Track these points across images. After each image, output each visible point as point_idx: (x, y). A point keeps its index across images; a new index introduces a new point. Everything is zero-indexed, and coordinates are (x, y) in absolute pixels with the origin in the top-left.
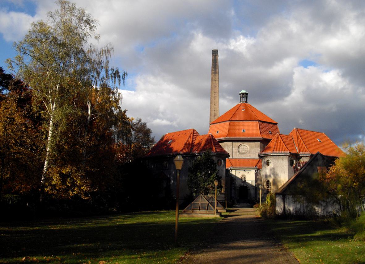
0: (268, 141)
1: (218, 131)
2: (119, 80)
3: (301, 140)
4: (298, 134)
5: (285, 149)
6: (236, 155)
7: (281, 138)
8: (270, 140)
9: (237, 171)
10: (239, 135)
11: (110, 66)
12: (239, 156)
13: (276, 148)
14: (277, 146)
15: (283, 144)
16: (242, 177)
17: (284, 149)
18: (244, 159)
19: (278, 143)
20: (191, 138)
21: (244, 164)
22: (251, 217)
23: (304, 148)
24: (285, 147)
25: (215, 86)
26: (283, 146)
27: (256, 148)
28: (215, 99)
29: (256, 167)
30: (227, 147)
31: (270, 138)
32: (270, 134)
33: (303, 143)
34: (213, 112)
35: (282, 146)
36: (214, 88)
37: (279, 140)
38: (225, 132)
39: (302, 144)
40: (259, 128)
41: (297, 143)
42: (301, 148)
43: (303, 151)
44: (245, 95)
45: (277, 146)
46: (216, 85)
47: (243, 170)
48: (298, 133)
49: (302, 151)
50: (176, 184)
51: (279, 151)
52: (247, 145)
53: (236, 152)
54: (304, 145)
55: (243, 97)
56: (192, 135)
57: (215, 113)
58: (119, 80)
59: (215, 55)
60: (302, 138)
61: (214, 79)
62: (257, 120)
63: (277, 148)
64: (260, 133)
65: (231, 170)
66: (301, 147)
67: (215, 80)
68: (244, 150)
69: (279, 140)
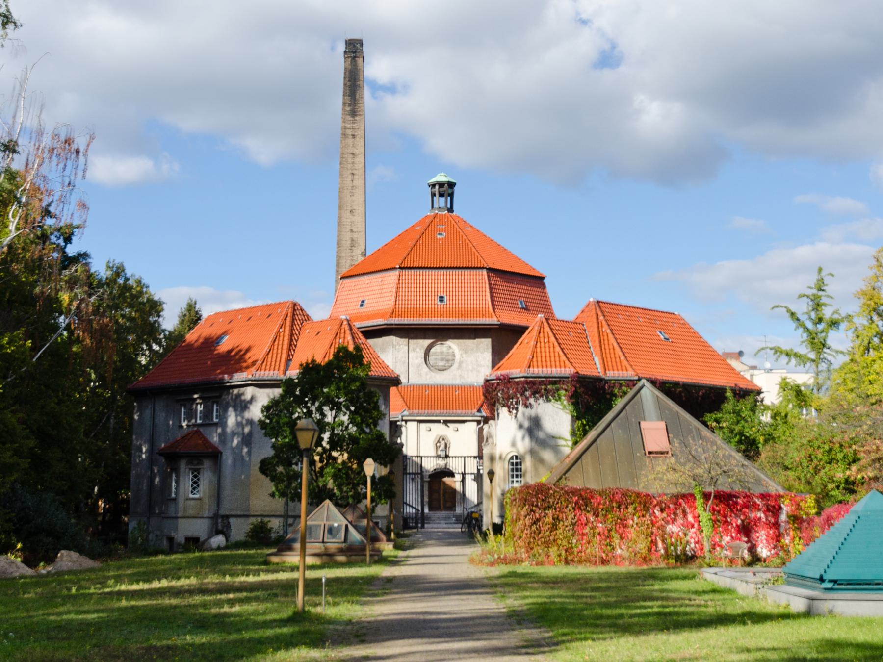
0: (518, 331)
1: (363, 301)
3: (611, 336)
4: (601, 318)
5: (562, 364)
7: (551, 329)
8: (527, 328)
9: (423, 425)
12: (428, 376)
13: (535, 359)
14: (539, 355)
15: (558, 349)
16: (438, 442)
17: (558, 364)
19: (543, 345)
20: (288, 328)
21: (441, 404)
23: (618, 360)
24: (563, 358)
25: (353, 154)
26: (557, 355)
30: (395, 356)
31: (523, 323)
32: (523, 308)
33: (615, 344)
34: (347, 236)
35: (552, 355)
36: (350, 160)
37: (546, 335)
38: (386, 302)
39: (611, 347)
42: (609, 359)
43: (615, 368)
44: (446, 190)
45: (539, 355)
46: (355, 151)
47: (439, 421)
48: (600, 313)
49: (611, 368)
51: (545, 369)
55: (441, 195)
56: (289, 319)
57: (352, 240)
59: (355, 57)
61: (349, 132)
62: (483, 268)
64: (491, 307)
65: (406, 421)
66: (608, 355)
67: (353, 136)
68: (442, 360)
69: (546, 335)
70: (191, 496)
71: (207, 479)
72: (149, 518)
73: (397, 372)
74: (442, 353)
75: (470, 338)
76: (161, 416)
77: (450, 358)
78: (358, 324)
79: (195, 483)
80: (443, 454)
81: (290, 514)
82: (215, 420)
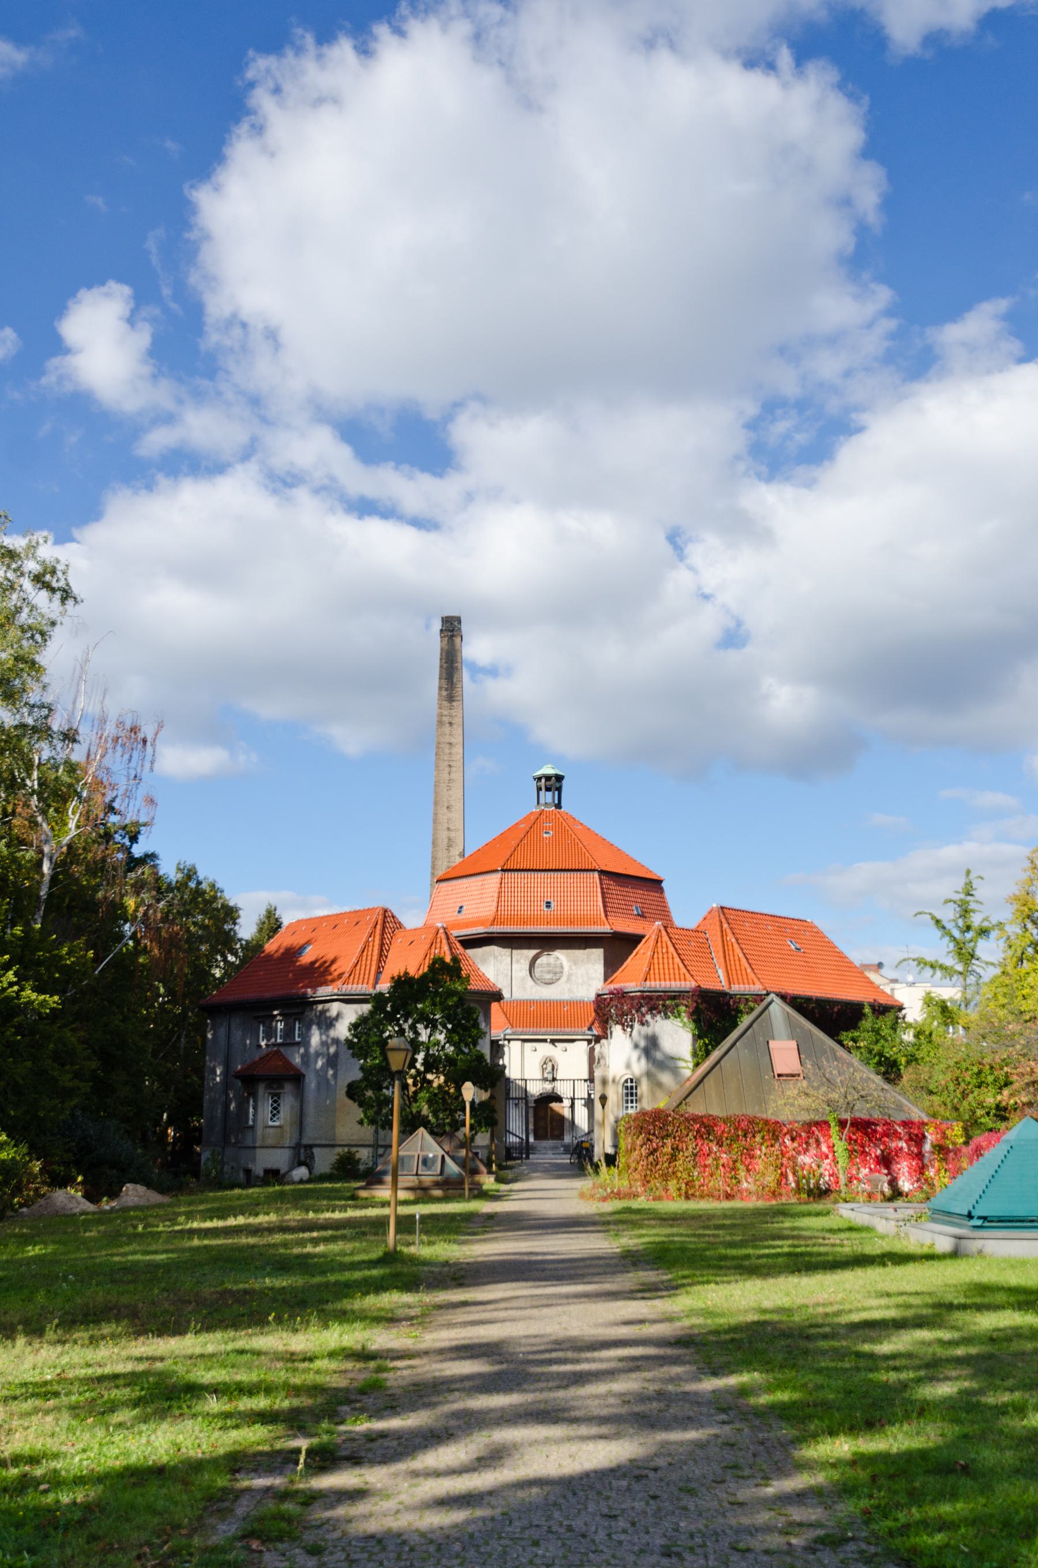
1: (461, 907)
3: (736, 946)
4: (725, 926)
5: (682, 977)
6: (525, 989)
7: (670, 938)
8: (643, 937)
9: (527, 1045)
10: (537, 920)
12: (534, 990)
13: (652, 972)
14: (656, 966)
15: (677, 960)
19: (660, 956)
20: (378, 937)
21: (547, 1022)
24: (683, 970)
26: (676, 966)
27: (590, 966)
28: (449, 788)
29: (590, 1029)
30: (497, 969)
34: (443, 835)
36: (447, 751)
40: (599, 895)
41: (721, 954)
42: (734, 972)
44: (553, 783)
45: (656, 966)
46: (453, 740)
47: (545, 1041)
48: (723, 920)
53: (523, 979)
54: (744, 961)
55: (548, 789)
56: (379, 927)
57: (449, 839)
59: (452, 636)
60: (737, 939)
61: (446, 719)
62: (594, 870)
63: (657, 971)
65: (509, 1040)
67: (451, 724)
68: (549, 972)
69: (664, 945)
70: (271, 1123)
71: (288, 1104)
72: (223, 1148)
73: (499, 985)
74: (549, 965)
75: (580, 948)
76: (237, 1034)
77: (558, 970)
78: (455, 933)
79: (275, 1109)
80: (550, 1077)
81: (380, 1143)
82: (297, 1039)
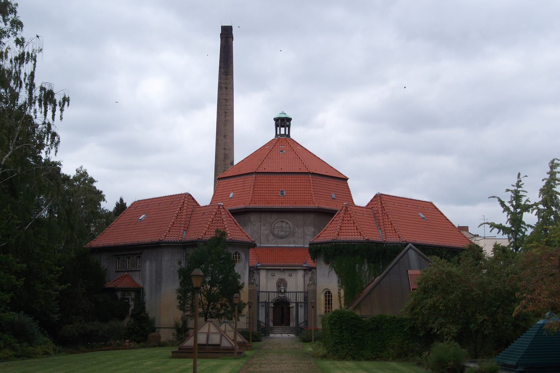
2: (54, 111)
11: (38, 82)
12: (274, 241)
18: (351, 242)
22: (99, 246)
25: (226, 100)
31: (334, 208)
50: (6, 131)
52: (289, 223)
58: (54, 111)
59: (228, 37)
67: (226, 88)
68: (282, 231)
80: (283, 291)
